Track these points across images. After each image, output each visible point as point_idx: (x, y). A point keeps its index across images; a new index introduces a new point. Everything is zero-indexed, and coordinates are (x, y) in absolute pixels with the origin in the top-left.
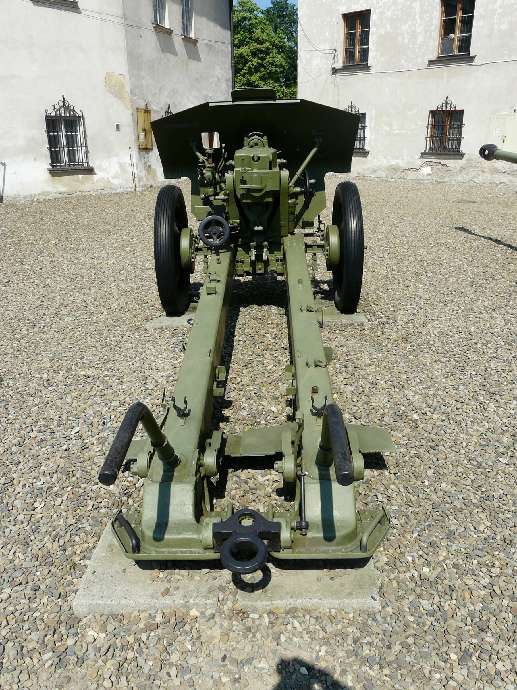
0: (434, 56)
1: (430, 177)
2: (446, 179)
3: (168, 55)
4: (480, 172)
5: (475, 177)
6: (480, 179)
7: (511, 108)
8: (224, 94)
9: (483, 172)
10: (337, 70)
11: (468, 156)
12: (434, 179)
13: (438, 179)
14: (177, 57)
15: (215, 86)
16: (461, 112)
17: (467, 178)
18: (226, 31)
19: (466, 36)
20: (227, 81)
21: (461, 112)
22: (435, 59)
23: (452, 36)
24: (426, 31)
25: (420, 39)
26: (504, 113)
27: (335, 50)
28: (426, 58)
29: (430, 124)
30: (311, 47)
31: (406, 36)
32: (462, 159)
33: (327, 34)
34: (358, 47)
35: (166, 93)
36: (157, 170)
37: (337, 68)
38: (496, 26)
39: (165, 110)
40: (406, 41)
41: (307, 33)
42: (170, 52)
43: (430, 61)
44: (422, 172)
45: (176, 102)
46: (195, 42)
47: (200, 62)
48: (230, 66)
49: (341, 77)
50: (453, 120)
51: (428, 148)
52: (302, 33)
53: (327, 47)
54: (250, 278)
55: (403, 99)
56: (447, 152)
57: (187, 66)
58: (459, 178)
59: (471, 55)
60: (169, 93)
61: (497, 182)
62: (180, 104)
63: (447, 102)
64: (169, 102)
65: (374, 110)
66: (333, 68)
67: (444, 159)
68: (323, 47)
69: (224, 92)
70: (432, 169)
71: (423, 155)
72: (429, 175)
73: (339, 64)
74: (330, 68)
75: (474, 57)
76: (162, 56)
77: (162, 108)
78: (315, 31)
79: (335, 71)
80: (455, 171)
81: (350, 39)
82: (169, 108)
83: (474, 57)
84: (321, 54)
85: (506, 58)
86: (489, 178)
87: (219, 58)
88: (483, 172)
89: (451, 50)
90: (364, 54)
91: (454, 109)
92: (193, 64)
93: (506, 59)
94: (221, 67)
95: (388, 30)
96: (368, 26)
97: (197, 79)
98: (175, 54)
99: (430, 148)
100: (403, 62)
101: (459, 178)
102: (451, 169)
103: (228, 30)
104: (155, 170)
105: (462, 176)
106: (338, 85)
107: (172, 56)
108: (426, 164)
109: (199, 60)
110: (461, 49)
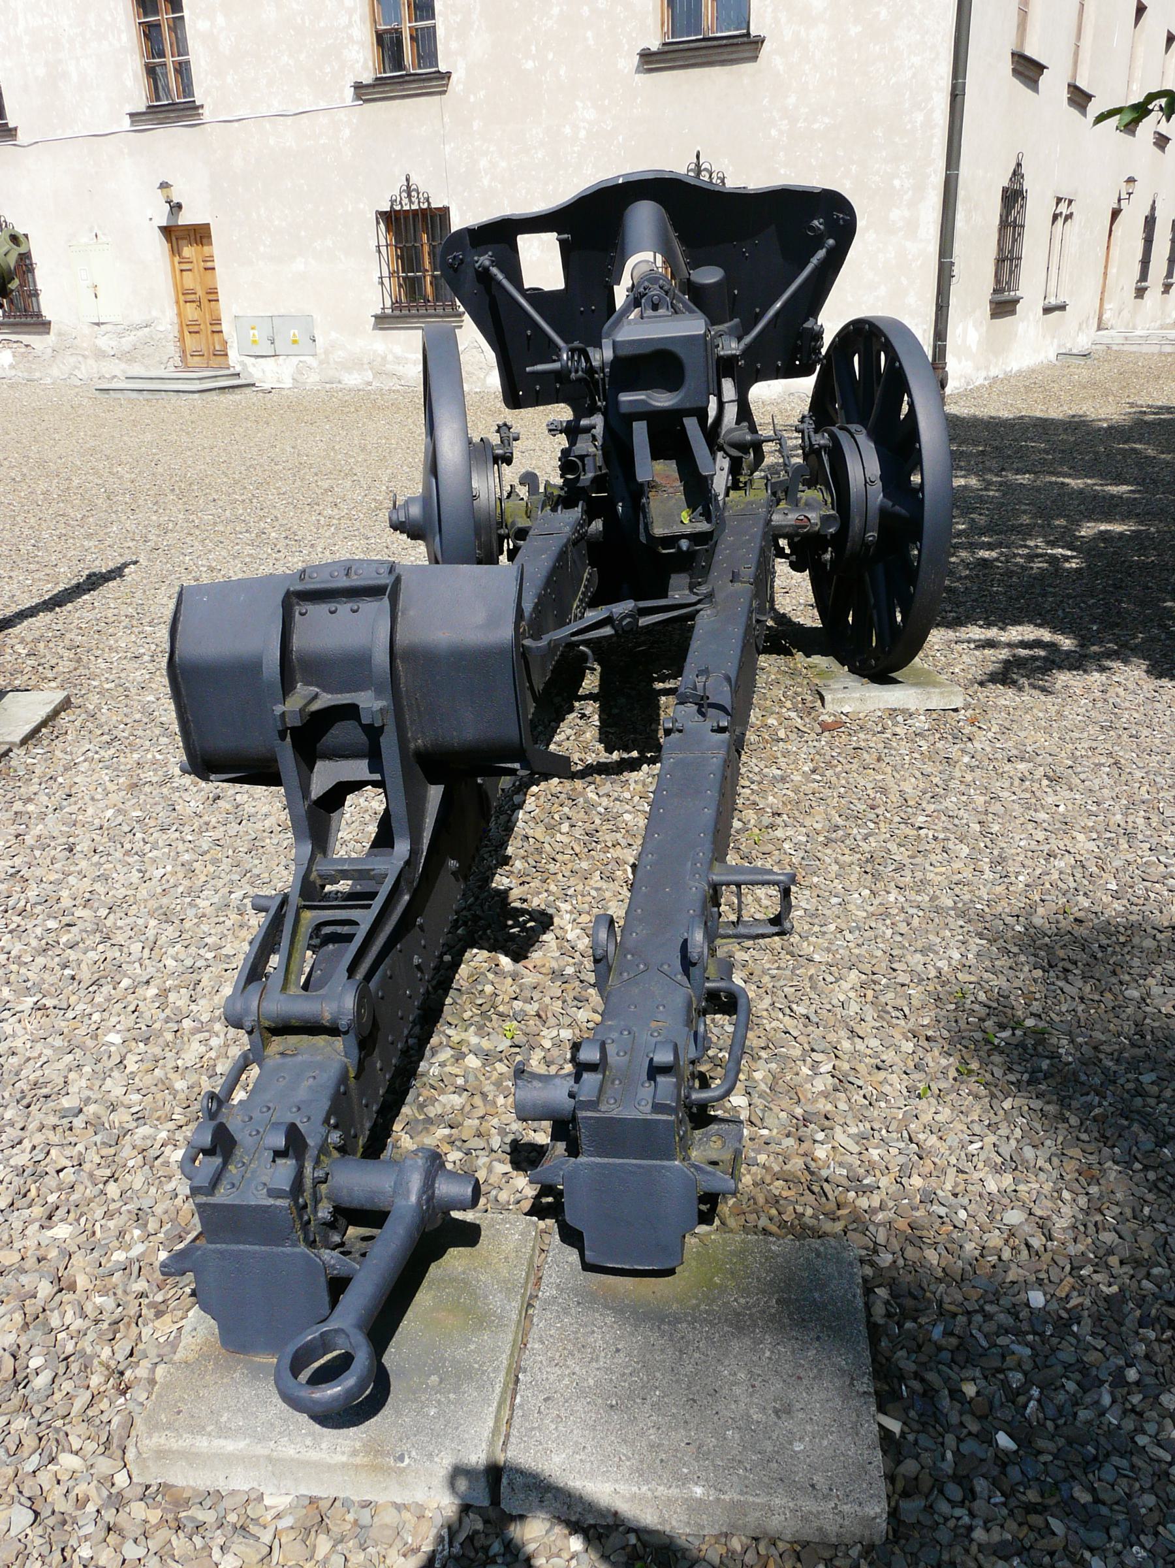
7: (91, 230)
63: (408, 187)
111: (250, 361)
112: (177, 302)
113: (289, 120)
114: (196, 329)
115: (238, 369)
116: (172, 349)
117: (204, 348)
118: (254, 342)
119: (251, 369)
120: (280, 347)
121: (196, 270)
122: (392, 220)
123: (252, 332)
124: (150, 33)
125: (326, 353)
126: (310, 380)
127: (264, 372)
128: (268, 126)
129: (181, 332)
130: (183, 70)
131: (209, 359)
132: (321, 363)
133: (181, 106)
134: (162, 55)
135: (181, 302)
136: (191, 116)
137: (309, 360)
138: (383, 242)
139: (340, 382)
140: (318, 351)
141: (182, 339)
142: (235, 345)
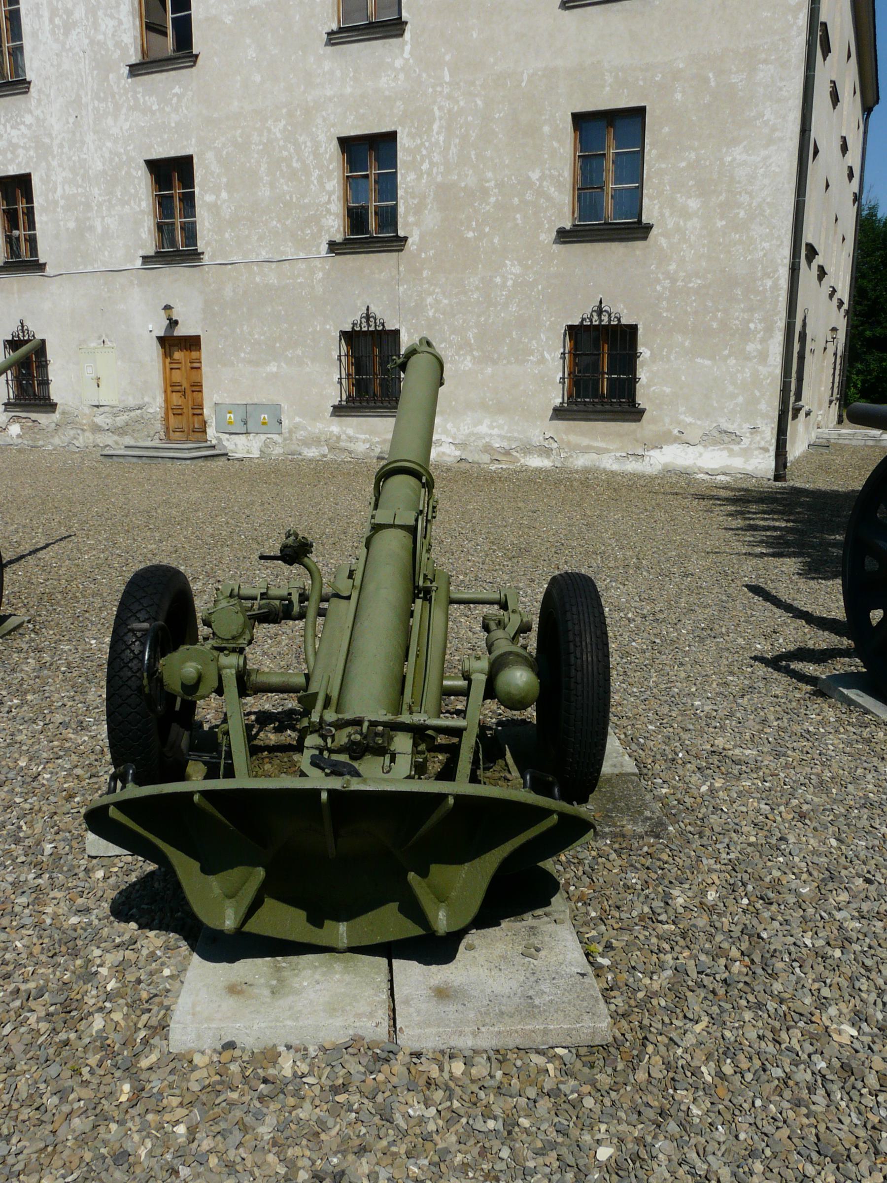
1: (20, 441)
2: (41, 443)
4: (79, 432)
5: (75, 438)
6: (80, 442)
7: (100, 338)
9: (82, 430)
11: (62, 407)
12: (26, 442)
13: (30, 443)
17: (66, 439)
19: (387, 206)
23: (16, 233)
29: (343, 353)
32: (54, 412)
34: (178, 221)
38: (62, 223)
44: (10, 432)
51: (344, 398)
56: (608, 407)
58: (56, 441)
59: (41, 261)
61: (101, 445)
63: (367, 315)
67: (34, 412)
70: (22, 429)
71: (8, 405)
72: (19, 436)
75: (45, 264)
80: (49, 429)
81: (164, 205)
83: (45, 264)
86: (91, 440)
88: (82, 430)
89: (173, 243)
90: (191, 233)
91: (381, 328)
93: (81, 269)
96: (32, 202)
99: (349, 396)
101: (56, 441)
102: (45, 427)
105: (59, 437)
108: (14, 419)
110: (381, 227)
112: (165, 392)
113: (274, 265)
114: (179, 411)
115: (214, 442)
116: (159, 426)
119: (225, 443)
121: (183, 368)
123: (228, 415)
127: (236, 445)
129: (167, 413)
130: (32, 241)
131: (188, 434)
132: (285, 439)
137: (276, 437)
139: (300, 454)
141: (166, 419)
142: (214, 424)
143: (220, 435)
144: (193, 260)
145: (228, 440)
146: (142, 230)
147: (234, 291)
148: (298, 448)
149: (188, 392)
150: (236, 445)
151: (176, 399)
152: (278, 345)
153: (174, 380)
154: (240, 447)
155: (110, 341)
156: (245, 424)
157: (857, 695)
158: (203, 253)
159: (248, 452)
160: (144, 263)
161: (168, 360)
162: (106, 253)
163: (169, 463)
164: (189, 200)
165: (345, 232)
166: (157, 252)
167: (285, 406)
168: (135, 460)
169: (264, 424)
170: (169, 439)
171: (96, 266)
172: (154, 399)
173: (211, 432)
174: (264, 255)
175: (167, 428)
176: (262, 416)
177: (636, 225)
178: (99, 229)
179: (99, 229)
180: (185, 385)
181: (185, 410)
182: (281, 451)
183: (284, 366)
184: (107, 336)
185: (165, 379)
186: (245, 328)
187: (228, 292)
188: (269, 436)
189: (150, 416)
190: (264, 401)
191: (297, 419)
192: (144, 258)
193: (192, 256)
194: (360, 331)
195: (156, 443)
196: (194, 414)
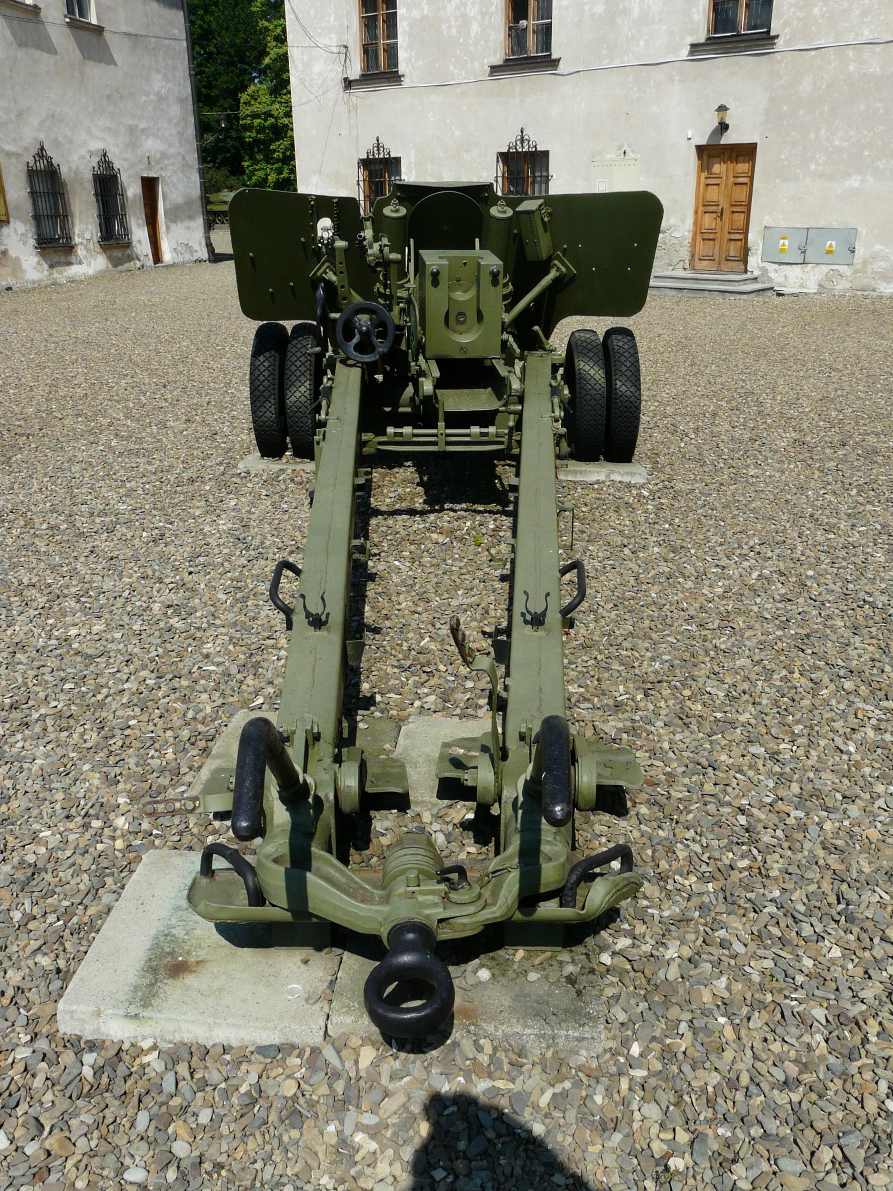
0: (498, 59)
3: (36, 53)
7: (620, 148)
8: (176, 125)
10: (350, 82)
14: (58, 57)
15: (154, 109)
16: (546, 154)
18: (174, 11)
20: (181, 101)
21: (546, 154)
22: (500, 62)
23: (523, 23)
24: (483, 14)
25: (475, 28)
26: (608, 157)
27: (346, 47)
28: (486, 61)
30: (308, 42)
31: (453, 23)
33: (332, 19)
35: (35, 122)
36: (23, 261)
37: (352, 78)
38: (587, 7)
39: (34, 150)
40: (454, 31)
41: (300, 16)
42: (38, 47)
43: (492, 67)
45: (60, 138)
46: (99, 30)
47: (112, 67)
48: (187, 73)
49: (358, 94)
50: (538, 169)
52: (293, 16)
53: (332, 41)
54: (409, 410)
55: (456, 133)
57: (82, 73)
59: (553, 57)
60: (42, 122)
62: (71, 141)
63: (522, 137)
64: (42, 136)
65: (413, 152)
66: (346, 79)
68: (327, 42)
69: (176, 121)
73: (355, 71)
74: (340, 77)
75: (558, 60)
76: (20, 54)
77: (26, 149)
78: (312, 12)
79: (348, 84)
82: (42, 149)
83: (558, 60)
84: (325, 54)
85: (605, 62)
87: (160, 59)
90: (392, 52)
92: (96, 71)
94: (165, 76)
95: (425, 12)
97: (109, 97)
98: (51, 50)
100: (451, 68)
103: (177, 8)
104: (17, 259)
106: (356, 107)
107: (45, 54)
109: (111, 61)
111: (771, 267)
112: (696, 212)
113: (878, 48)
114: (711, 236)
115: (757, 273)
116: (685, 254)
117: (716, 253)
118: (782, 250)
119: (772, 275)
120: (809, 257)
121: (723, 186)
122: (366, 163)
123: (782, 241)
124: (369, 24)
125: (865, 263)
126: (840, 287)
127: (786, 277)
128: (851, 53)
129: (694, 239)
130: (546, 32)
131: (719, 263)
132: (856, 272)
133: (746, 38)
134: (376, 38)
135: (700, 213)
136: (764, 45)
137: (843, 269)
138: (361, 178)
139: (874, 290)
140: (855, 261)
141: (693, 245)
142: (760, 252)
143: (766, 264)
144: (763, 46)
145: (776, 271)
146: (694, 10)
147: (814, 84)
148: (873, 283)
149: (726, 214)
150: (786, 277)
151: (709, 221)
152: (866, 153)
153: (709, 198)
154: (791, 280)
155: (633, 152)
156: (804, 252)
157: (628, 473)
158: (777, 37)
159: (801, 286)
160: (691, 53)
161: (704, 175)
162: (642, 43)
163: (719, 298)
164: (391, 21)
165: (708, 30)
166: (709, 39)
167: (863, 231)
168: (673, 292)
169: (829, 252)
170: (693, 268)
171: (626, 59)
172: (683, 221)
173: (754, 262)
174: (867, 34)
175: (693, 256)
176: (829, 243)
177: (764, 36)
178: (636, 13)
179: (636, 13)
180: (724, 204)
181: (718, 235)
182: (848, 286)
183: (871, 180)
184: (630, 145)
185: (697, 197)
186: (823, 132)
187: (805, 87)
188: (834, 267)
189: (674, 241)
190: (835, 224)
191: (878, 247)
192: (693, 46)
193: (392, 77)
194: (374, 159)
195: (680, 273)
196: (731, 240)
